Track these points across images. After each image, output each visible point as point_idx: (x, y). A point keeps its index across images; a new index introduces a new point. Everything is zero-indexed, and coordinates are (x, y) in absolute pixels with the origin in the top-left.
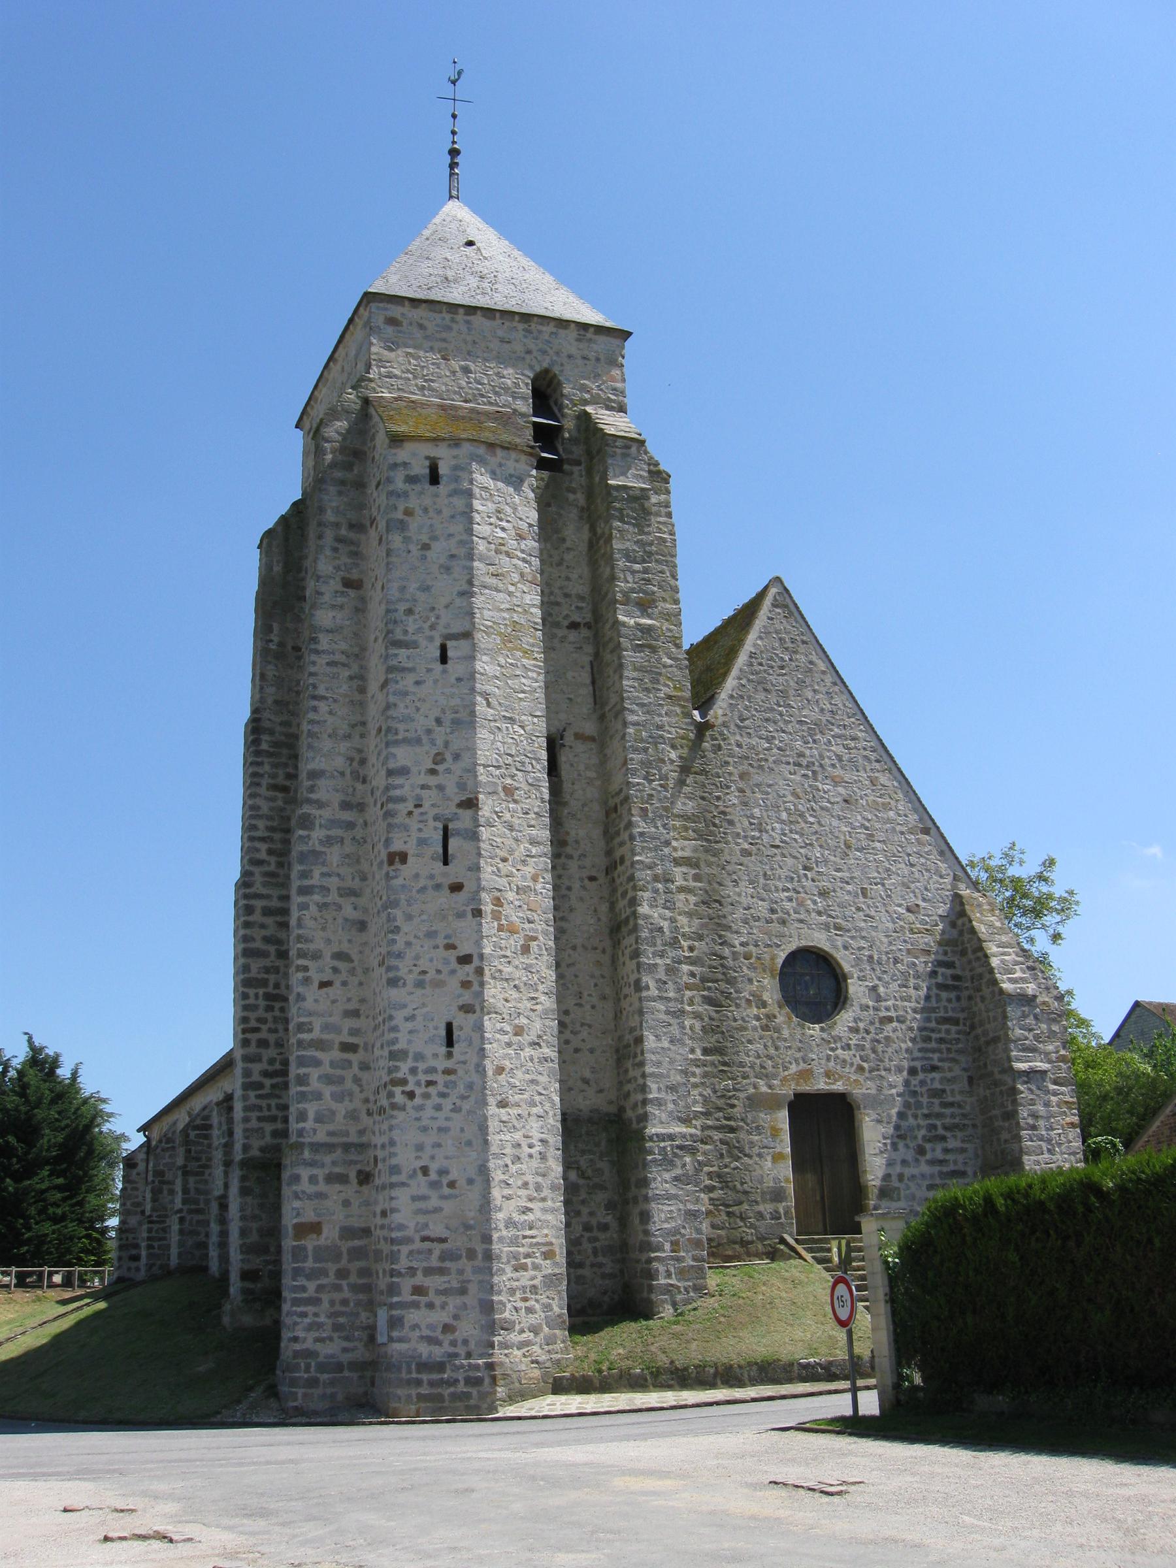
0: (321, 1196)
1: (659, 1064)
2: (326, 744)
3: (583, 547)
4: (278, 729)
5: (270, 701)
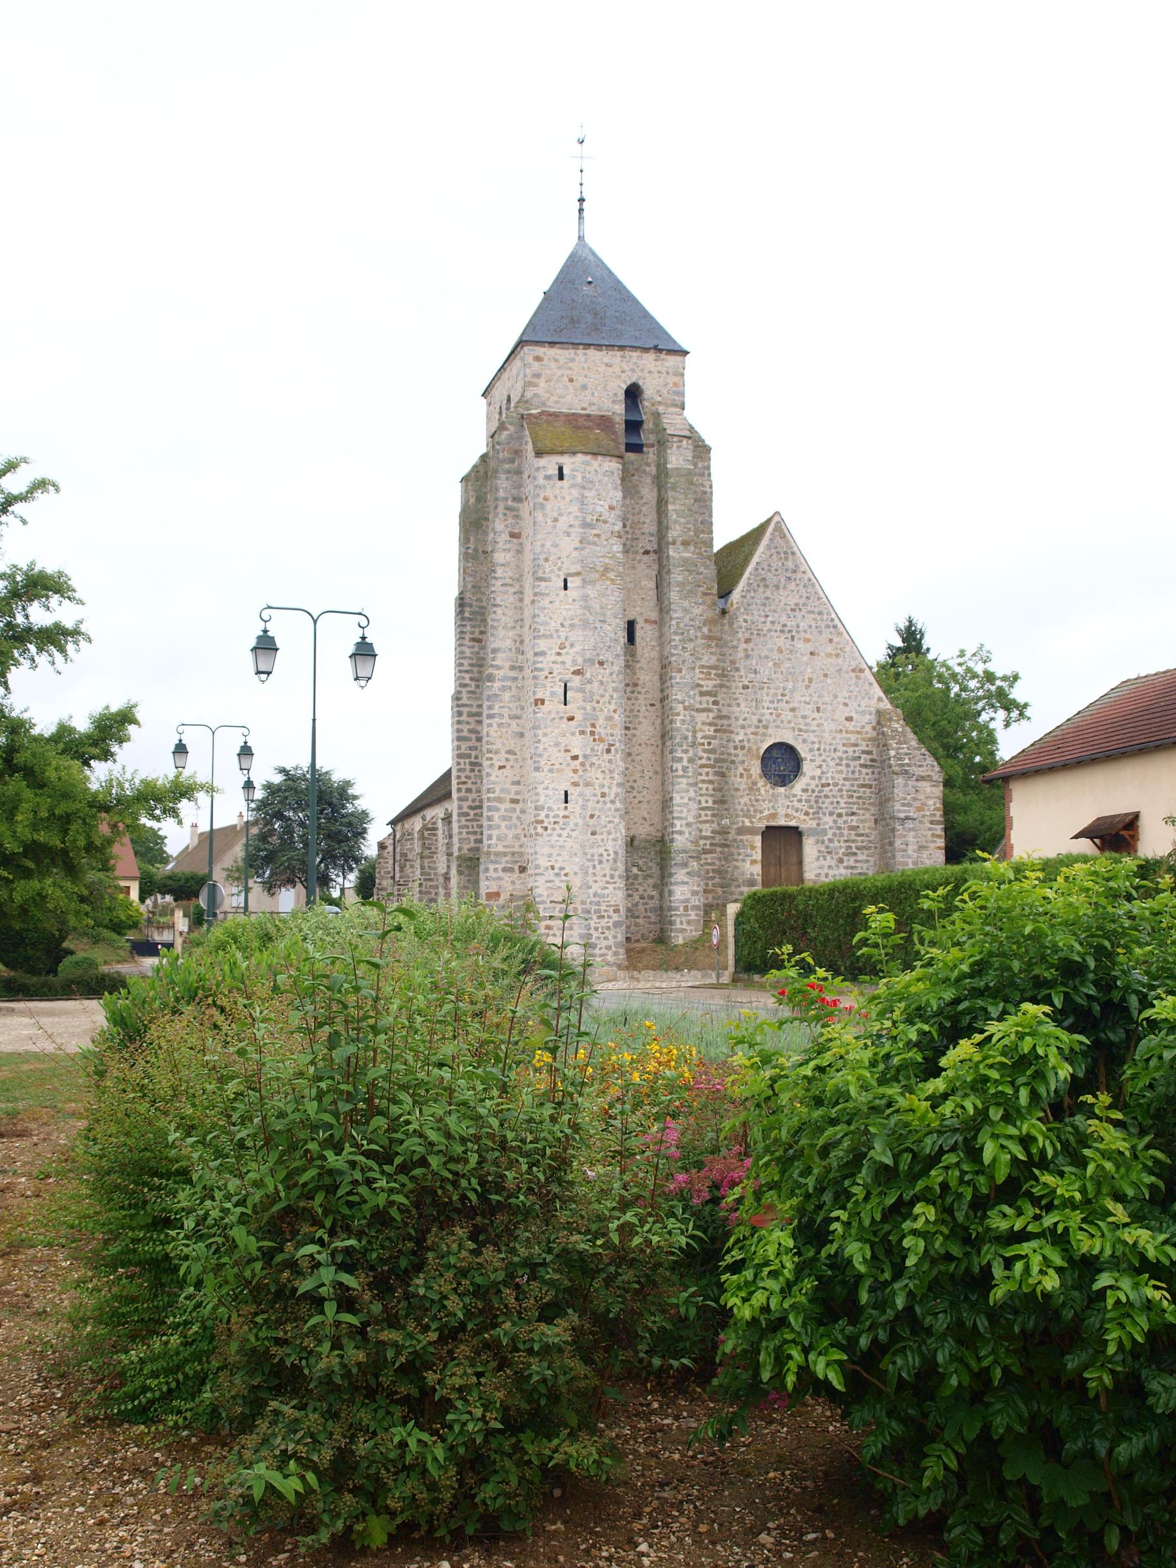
0: (500, 878)
2: (501, 633)
3: (654, 502)
4: (475, 604)
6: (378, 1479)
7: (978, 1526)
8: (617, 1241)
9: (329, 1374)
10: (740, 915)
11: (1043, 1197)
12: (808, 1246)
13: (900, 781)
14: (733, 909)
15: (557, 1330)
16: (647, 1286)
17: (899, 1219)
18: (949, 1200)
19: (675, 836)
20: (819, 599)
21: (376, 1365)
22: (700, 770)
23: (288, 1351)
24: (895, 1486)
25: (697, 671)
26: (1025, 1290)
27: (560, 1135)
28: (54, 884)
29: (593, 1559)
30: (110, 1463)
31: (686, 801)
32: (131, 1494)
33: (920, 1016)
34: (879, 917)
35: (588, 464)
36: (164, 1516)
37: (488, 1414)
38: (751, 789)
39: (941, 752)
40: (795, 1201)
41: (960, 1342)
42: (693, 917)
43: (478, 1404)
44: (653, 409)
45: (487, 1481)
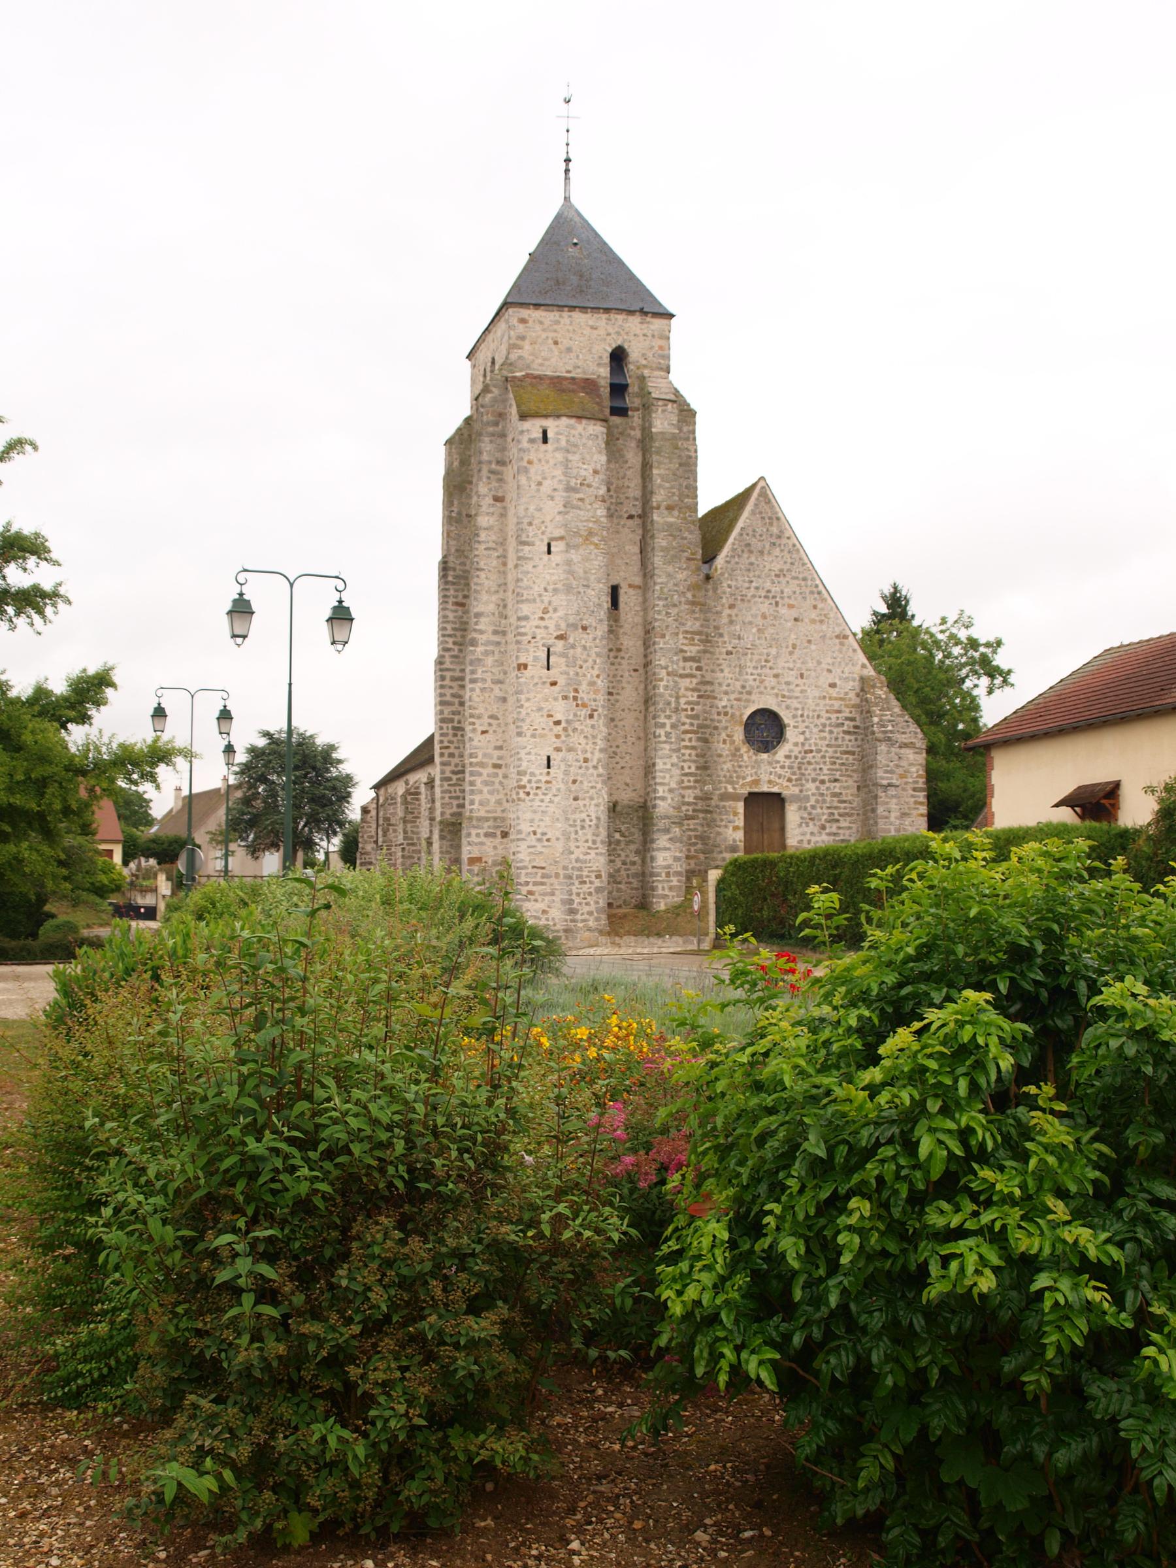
0: (482, 844)
1: (664, 778)
2: (484, 597)
3: (638, 466)
4: (458, 567)
5: (453, 550)
6: (301, 1476)
7: (916, 1527)
8: (548, 1233)
9: (249, 1368)
10: (721, 881)
11: (981, 1192)
12: (746, 1238)
13: (883, 748)
14: (714, 875)
15: (484, 1323)
16: (583, 1277)
17: (835, 1213)
18: (885, 1194)
19: (658, 802)
20: (804, 564)
21: (297, 1358)
22: (683, 736)
23: (208, 1343)
24: (833, 1483)
25: (681, 636)
26: (959, 1290)
27: (495, 1120)
28: (31, 848)
29: (521, 1558)
30: (38, 1451)
31: (668, 766)
32: (57, 1484)
33: (864, 1000)
34: (823, 897)
35: (573, 428)
36: (88, 1508)
37: (411, 1411)
38: (734, 755)
39: (924, 718)
40: (731, 1191)
41: (896, 1341)
42: (675, 883)
43: (402, 1400)
44: (639, 372)
45: (413, 1478)
